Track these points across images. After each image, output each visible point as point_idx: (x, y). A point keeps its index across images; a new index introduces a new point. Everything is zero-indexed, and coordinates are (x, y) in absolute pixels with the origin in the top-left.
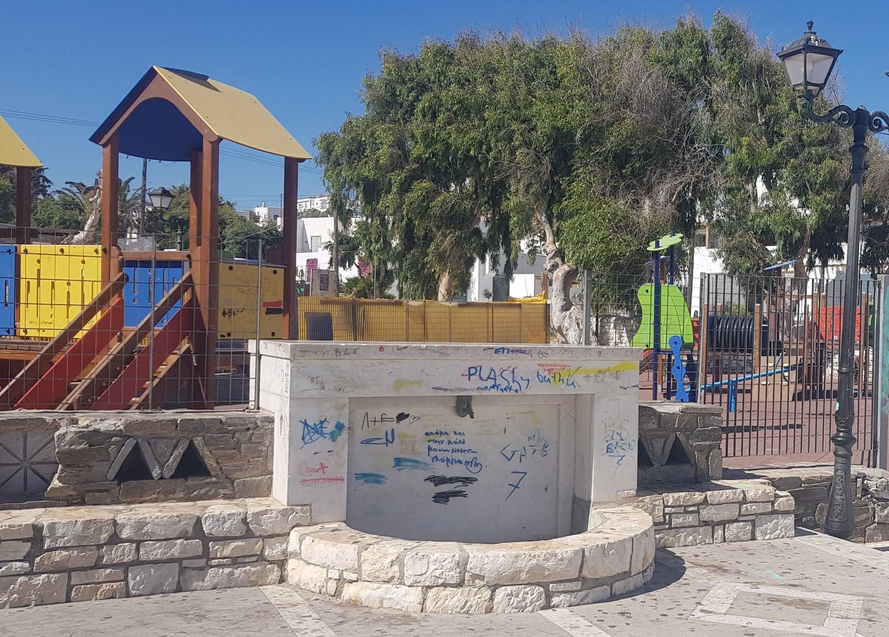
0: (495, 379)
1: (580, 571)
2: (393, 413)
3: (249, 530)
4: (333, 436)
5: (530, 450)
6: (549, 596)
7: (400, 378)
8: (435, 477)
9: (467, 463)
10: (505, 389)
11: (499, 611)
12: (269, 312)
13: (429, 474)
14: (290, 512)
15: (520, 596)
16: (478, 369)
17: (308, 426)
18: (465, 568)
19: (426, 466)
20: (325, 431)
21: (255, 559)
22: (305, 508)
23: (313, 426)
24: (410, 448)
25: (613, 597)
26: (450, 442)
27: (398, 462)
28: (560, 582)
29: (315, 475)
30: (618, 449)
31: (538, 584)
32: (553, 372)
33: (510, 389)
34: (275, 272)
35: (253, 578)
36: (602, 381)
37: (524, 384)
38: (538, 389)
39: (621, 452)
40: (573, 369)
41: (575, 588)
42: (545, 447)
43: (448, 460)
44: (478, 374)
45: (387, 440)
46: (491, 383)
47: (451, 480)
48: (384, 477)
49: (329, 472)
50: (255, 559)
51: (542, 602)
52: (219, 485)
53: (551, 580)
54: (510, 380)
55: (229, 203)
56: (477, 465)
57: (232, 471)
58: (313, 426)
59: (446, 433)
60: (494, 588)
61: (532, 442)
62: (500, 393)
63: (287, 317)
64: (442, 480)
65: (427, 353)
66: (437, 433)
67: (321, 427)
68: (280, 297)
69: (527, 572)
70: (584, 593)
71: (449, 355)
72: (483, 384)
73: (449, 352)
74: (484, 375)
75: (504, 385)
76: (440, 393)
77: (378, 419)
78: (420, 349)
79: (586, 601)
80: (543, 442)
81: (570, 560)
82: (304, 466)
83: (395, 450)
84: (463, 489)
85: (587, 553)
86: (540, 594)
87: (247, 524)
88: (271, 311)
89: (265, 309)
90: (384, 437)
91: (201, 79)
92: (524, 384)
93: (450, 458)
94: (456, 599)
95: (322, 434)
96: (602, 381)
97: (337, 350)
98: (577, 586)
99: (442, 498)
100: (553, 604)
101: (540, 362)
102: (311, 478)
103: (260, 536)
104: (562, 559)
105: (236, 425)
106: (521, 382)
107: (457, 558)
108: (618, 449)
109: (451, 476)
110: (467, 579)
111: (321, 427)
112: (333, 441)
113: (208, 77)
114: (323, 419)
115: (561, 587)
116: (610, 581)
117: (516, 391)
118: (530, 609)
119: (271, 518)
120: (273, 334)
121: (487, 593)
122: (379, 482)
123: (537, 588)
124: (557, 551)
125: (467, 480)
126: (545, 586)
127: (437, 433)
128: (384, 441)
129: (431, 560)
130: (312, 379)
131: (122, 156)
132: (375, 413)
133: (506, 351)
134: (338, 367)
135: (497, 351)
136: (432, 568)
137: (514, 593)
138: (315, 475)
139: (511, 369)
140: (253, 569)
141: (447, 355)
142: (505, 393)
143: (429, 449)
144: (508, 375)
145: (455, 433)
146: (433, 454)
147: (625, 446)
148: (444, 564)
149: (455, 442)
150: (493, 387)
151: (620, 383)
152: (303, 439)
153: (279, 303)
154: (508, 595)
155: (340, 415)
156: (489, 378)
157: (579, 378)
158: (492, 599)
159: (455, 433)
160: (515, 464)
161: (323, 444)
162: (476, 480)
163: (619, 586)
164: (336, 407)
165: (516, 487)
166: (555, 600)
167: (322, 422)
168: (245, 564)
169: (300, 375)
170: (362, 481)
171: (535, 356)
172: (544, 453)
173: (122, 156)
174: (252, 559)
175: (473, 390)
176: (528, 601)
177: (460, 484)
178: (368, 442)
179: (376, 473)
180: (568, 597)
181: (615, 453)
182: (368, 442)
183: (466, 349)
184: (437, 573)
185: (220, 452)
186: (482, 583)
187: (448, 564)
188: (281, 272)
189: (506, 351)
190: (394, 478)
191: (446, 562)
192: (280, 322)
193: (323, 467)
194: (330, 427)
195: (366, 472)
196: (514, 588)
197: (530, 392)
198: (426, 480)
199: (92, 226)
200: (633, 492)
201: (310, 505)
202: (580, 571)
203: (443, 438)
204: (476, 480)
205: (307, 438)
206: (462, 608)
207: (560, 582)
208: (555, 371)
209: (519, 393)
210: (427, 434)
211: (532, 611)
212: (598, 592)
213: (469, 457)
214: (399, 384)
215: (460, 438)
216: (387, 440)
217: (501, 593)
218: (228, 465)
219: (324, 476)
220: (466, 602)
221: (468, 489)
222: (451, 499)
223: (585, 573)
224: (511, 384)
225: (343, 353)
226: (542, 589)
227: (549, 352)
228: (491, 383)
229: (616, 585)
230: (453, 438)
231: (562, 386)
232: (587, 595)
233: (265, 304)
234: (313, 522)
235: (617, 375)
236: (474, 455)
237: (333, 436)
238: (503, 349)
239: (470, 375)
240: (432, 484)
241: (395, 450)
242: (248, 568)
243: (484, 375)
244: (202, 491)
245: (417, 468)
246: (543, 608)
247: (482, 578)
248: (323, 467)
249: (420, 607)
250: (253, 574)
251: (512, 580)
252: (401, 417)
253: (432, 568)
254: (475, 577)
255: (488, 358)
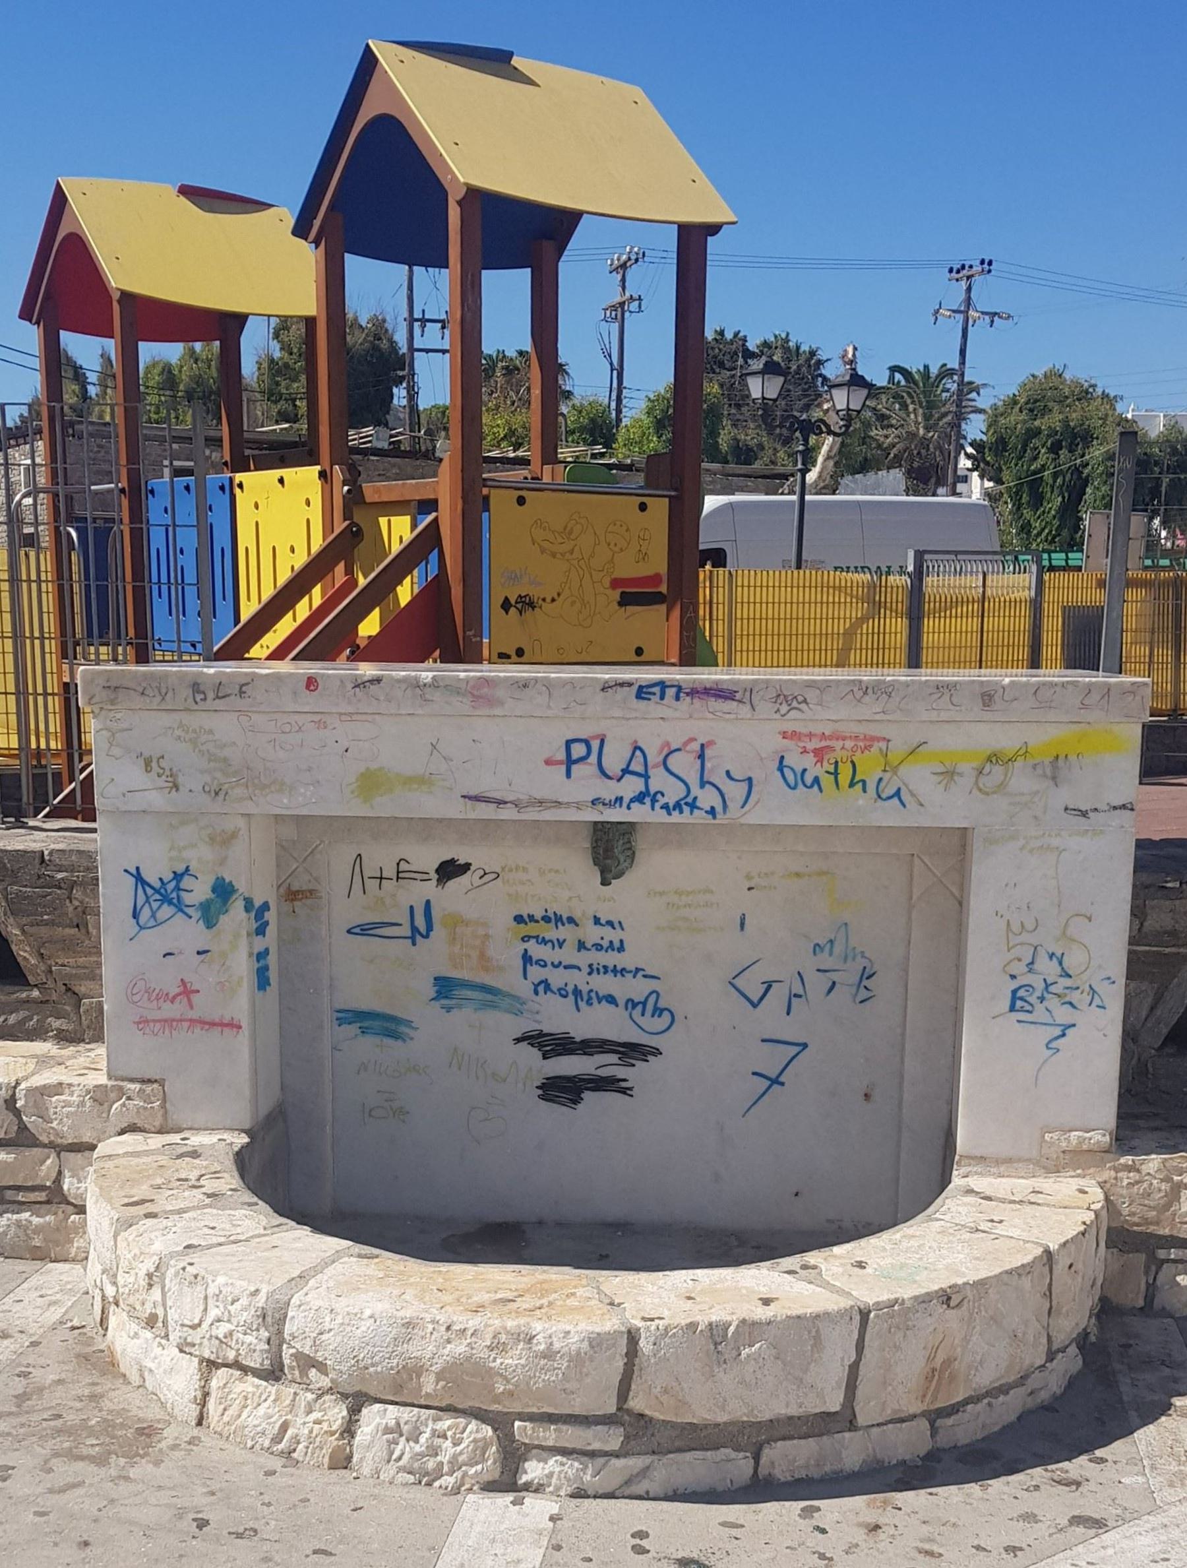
0: (646, 777)
1: (624, 1392)
2: (428, 858)
3: (23, 1128)
4: (209, 914)
5: (816, 984)
6: (513, 1456)
7: (374, 766)
8: (541, 1034)
9: (631, 1004)
10: (678, 806)
11: (366, 1470)
12: (626, 600)
13: (526, 1025)
14: (113, 1095)
15: (422, 1439)
16: (595, 745)
17: (144, 883)
18: (280, 1332)
19: (516, 1005)
20: (188, 898)
21: (42, 1196)
22: (148, 1088)
23: (157, 885)
24: (475, 954)
25: (760, 1489)
26: (581, 946)
27: (445, 987)
28: (551, 1419)
29: (170, 1010)
30: (1052, 1002)
31: (480, 1415)
32: (831, 757)
33: (693, 806)
34: (643, 507)
35: (37, 1242)
36: (1001, 787)
37: (735, 792)
38: (777, 807)
39: (1063, 1014)
40: (897, 751)
41: (596, 1446)
42: (867, 975)
43: (577, 992)
44: (593, 758)
45: (414, 929)
46: (631, 786)
47: (587, 1047)
48: (408, 1023)
49: (204, 1006)
50: (42, 1196)
51: (490, 1466)
52: (49, 1006)
53: (517, 1408)
54: (693, 780)
55: (1105, 396)
56: (658, 1011)
57: (77, 977)
58: (157, 885)
59: (571, 920)
60: (357, 1402)
61: (827, 961)
62: (660, 816)
63: (676, 613)
64: (560, 1045)
65: (437, 695)
66: (546, 919)
67: (178, 888)
68: (658, 564)
69: (440, 1376)
70: (635, 1463)
71: (501, 703)
72: (609, 790)
73: (500, 693)
74: (614, 760)
75: (673, 792)
76: (485, 811)
77: (390, 872)
78: (417, 685)
79: (640, 1489)
80: (860, 963)
81: (577, 1360)
82: (141, 984)
83: (436, 956)
84: (620, 1072)
85: (645, 1345)
86: (481, 1447)
87: (17, 1113)
88: (634, 595)
89: (616, 595)
90: (405, 920)
91: (495, 61)
92: (735, 792)
93: (584, 989)
94: (261, 1411)
95: (180, 907)
96: (1001, 787)
97: (196, 687)
98: (614, 1439)
99: (563, 1091)
100: (524, 1479)
101: (789, 727)
102: (158, 1015)
103: (51, 1145)
104: (549, 1354)
105: (72, 869)
106: (729, 787)
107: (261, 1301)
108: (1052, 1002)
109: (589, 1036)
110: (287, 1362)
111: (178, 888)
112: (210, 925)
113: (511, 54)
114: (180, 869)
115: (550, 1435)
116: (754, 1436)
117: (712, 812)
118: (449, 1481)
119: (67, 1104)
120: (639, 652)
121: (338, 1413)
122: (395, 1035)
123: (473, 1425)
124: (537, 1326)
125: (633, 1052)
126: (500, 1423)
127: (546, 919)
128: (406, 931)
129: (211, 1291)
130: (148, 763)
131: (352, 262)
132: (381, 857)
133: (671, 692)
134: (211, 732)
135: (642, 692)
136: (213, 1313)
137: (405, 1429)
138: (170, 1010)
139: (696, 746)
140: (36, 1220)
141: (491, 702)
142: (676, 817)
143: (527, 959)
144: (684, 764)
145: (597, 921)
146: (535, 973)
147: (1075, 997)
148: (232, 1308)
149: (598, 947)
150: (640, 798)
151: (1063, 796)
152: (135, 915)
153: (655, 579)
154: (387, 1430)
155: (223, 862)
156: (626, 771)
157: (918, 778)
158: (349, 1430)
159: (597, 921)
160: (771, 1018)
161: (184, 932)
162: (657, 1052)
163: (784, 1458)
164: (212, 839)
165: (776, 1081)
166: (533, 1470)
167: (178, 877)
168: (21, 1206)
169: (116, 751)
170: (353, 1029)
171: (765, 708)
172: (863, 994)
173: (352, 262)
174: (33, 1196)
175: (578, 806)
176: (444, 1458)
177: (613, 1058)
178: (364, 930)
179: (388, 1011)
180: (572, 1466)
181: (1040, 1013)
182: (364, 930)
183: (548, 685)
184: (222, 1329)
185: (44, 931)
186: (325, 1382)
187: (243, 1313)
188: (660, 508)
189: (671, 692)
190: (436, 1030)
191: (237, 1305)
192: (656, 625)
193: (187, 991)
194: (199, 891)
195: (364, 1005)
196: (407, 1414)
197: (755, 816)
198: (518, 1040)
199: (828, 458)
200: (1100, 1138)
201: (161, 1082)
202: (624, 1392)
203: (564, 932)
204: (657, 1052)
205: (145, 914)
206: (277, 1439)
207: (551, 1419)
208: (839, 754)
209: (721, 819)
210: (519, 919)
211: (456, 1491)
212: (693, 1466)
213: (638, 988)
214: (371, 782)
215: (612, 935)
216: (414, 929)
217: (373, 1418)
218: (64, 963)
219: (192, 1014)
220: (284, 1427)
221: (635, 1074)
222: (587, 1095)
223: (636, 1403)
224: (696, 791)
225: (211, 695)
226: (488, 1431)
227: (811, 695)
228: (631, 786)
229: (767, 1454)
230: (593, 934)
231: (861, 800)
232: (644, 1472)
233: (615, 583)
234: (170, 1124)
235: (1055, 768)
236: (653, 985)
237: (209, 914)
238: (662, 685)
239: (570, 762)
240: (536, 1053)
241: (436, 956)
242: (26, 1215)
243: (614, 760)
244: (12, 1019)
245: (493, 1006)
246: (491, 1487)
247: (322, 1368)
248: (187, 991)
249: (194, 1411)
250: (38, 1230)
251: (400, 1388)
252: (449, 870)
253: (213, 1313)
254: (307, 1362)
255: (618, 713)
